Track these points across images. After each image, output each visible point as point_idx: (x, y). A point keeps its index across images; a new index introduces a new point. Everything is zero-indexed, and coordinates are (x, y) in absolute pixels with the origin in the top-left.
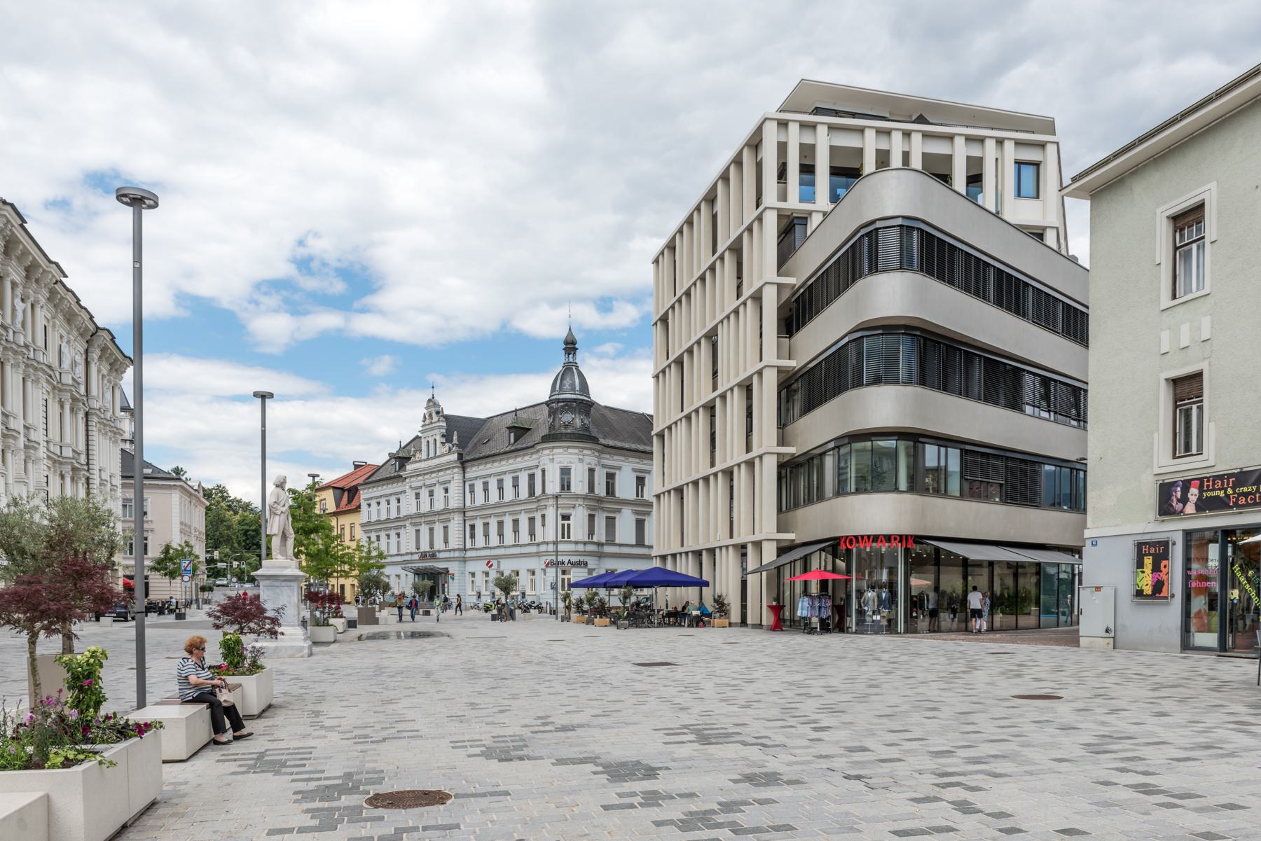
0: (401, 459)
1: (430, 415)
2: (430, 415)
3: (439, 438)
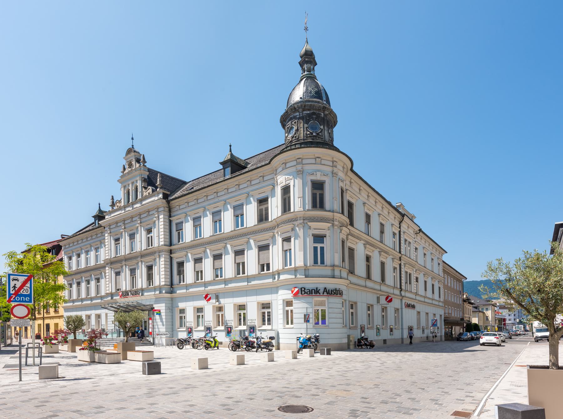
0: (100, 216)
1: (130, 165)
2: (130, 165)
3: (139, 184)
